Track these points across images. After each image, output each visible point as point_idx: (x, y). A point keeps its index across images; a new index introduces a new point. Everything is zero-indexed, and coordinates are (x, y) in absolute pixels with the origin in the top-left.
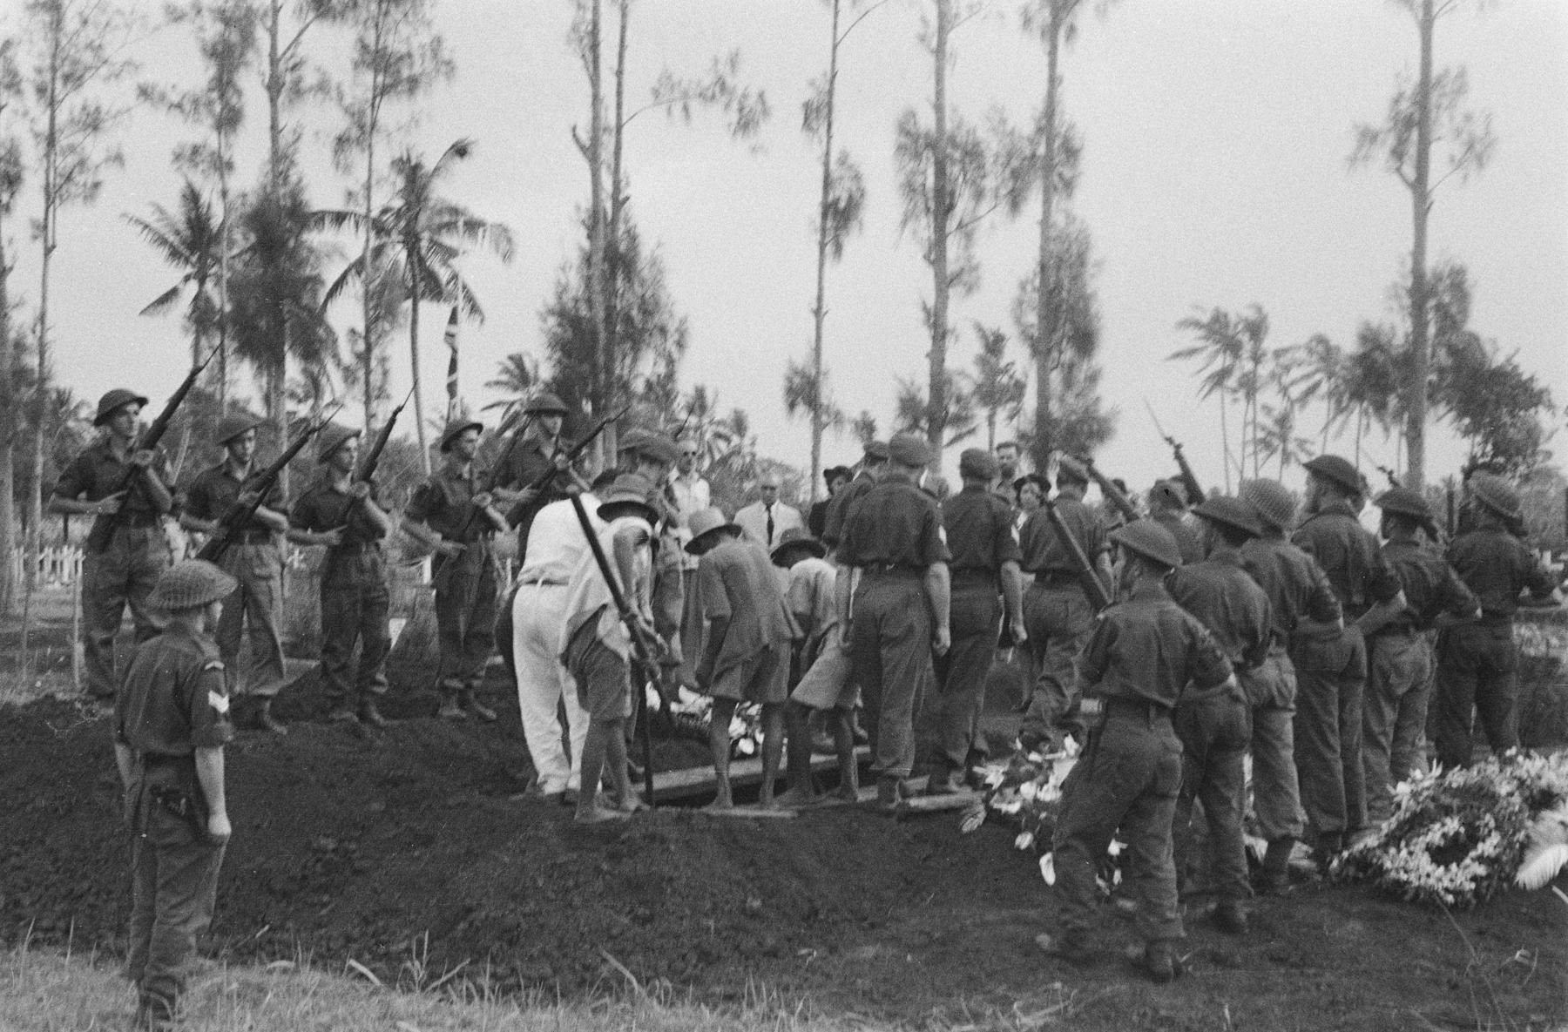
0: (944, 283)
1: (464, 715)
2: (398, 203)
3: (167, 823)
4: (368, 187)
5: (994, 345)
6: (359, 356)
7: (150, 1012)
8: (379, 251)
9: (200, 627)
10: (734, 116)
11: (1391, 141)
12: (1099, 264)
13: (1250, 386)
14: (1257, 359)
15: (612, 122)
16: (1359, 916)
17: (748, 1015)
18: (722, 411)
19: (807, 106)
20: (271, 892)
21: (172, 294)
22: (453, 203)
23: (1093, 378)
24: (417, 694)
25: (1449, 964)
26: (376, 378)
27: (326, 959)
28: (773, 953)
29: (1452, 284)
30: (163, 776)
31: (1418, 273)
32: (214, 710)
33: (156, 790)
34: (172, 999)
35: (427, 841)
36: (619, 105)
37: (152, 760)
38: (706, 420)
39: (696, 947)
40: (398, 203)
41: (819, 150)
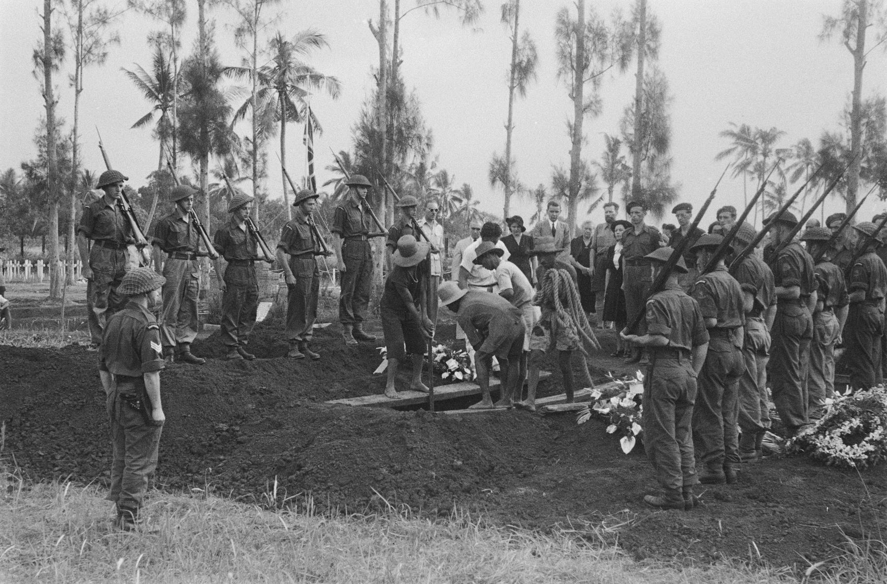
0: (580, 110)
1: (304, 356)
2: (273, 65)
3: (130, 414)
4: (254, 56)
5: (613, 147)
6: (250, 153)
7: (123, 518)
8: (262, 94)
9: (145, 305)
10: (463, 13)
11: (844, 26)
12: (670, 99)
13: (760, 169)
14: (765, 155)
15: (393, 18)
16: (800, 474)
17: (452, 524)
18: (456, 185)
19: (504, 7)
20: (193, 453)
21: (148, 117)
22: (306, 65)
23: (667, 164)
24: (276, 344)
25: (851, 501)
26: (259, 166)
27: (221, 491)
28: (468, 491)
29: (876, 110)
30: (127, 387)
31: (856, 105)
32: (154, 351)
33: (123, 396)
34: (135, 511)
35: (279, 426)
36: (397, 8)
37: (120, 379)
39: (426, 486)
40: (273, 65)
41: (510, 33)
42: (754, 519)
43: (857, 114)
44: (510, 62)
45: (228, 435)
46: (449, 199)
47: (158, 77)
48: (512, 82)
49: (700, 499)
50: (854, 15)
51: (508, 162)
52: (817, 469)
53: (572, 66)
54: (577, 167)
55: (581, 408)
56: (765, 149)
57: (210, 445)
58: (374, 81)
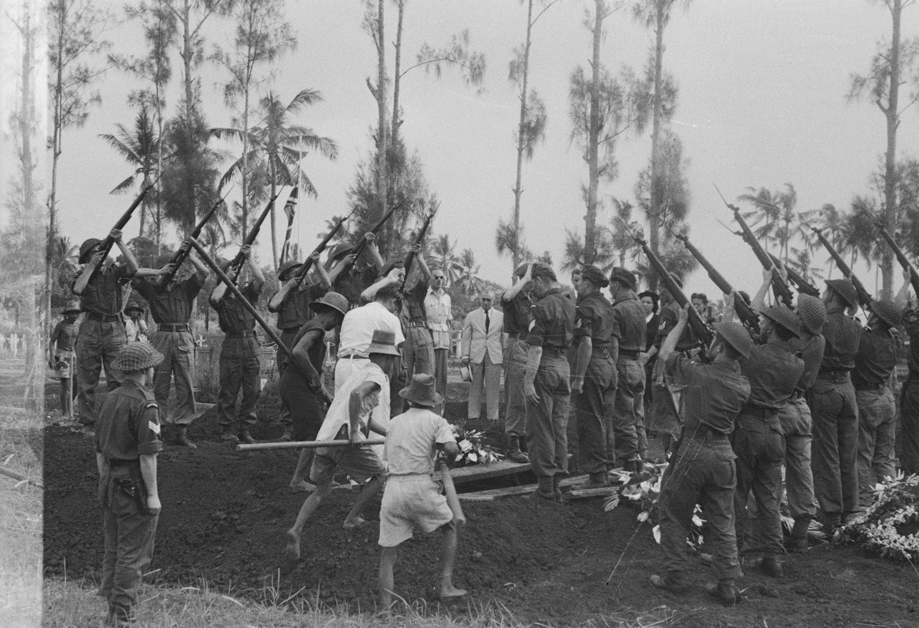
0: (595, 173)
2: (264, 126)
3: (124, 501)
4: (245, 116)
5: (624, 211)
6: (239, 218)
7: (115, 616)
8: (252, 156)
10: (467, 71)
11: (873, 84)
12: (688, 161)
14: (788, 219)
18: (458, 252)
20: (188, 544)
21: (128, 182)
28: (489, 585)
30: (122, 472)
31: (890, 167)
32: (152, 431)
33: (116, 481)
34: (127, 608)
36: (398, 65)
38: (448, 257)
41: (518, 92)
42: (805, 616)
43: (891, 177)
44: (518, 121)
45: (226, 524)
46: (449, 266)
47: (140, 139)
48: (521, 144)
49: (743, 594)
50: (885, 73)
51: (517, 227)
52: (871, 561)
53: (587, 127)
54: (592, 234)
55: (609, 494)
56: (787, 213)
57: (207, 535)
58: (374, 142)
